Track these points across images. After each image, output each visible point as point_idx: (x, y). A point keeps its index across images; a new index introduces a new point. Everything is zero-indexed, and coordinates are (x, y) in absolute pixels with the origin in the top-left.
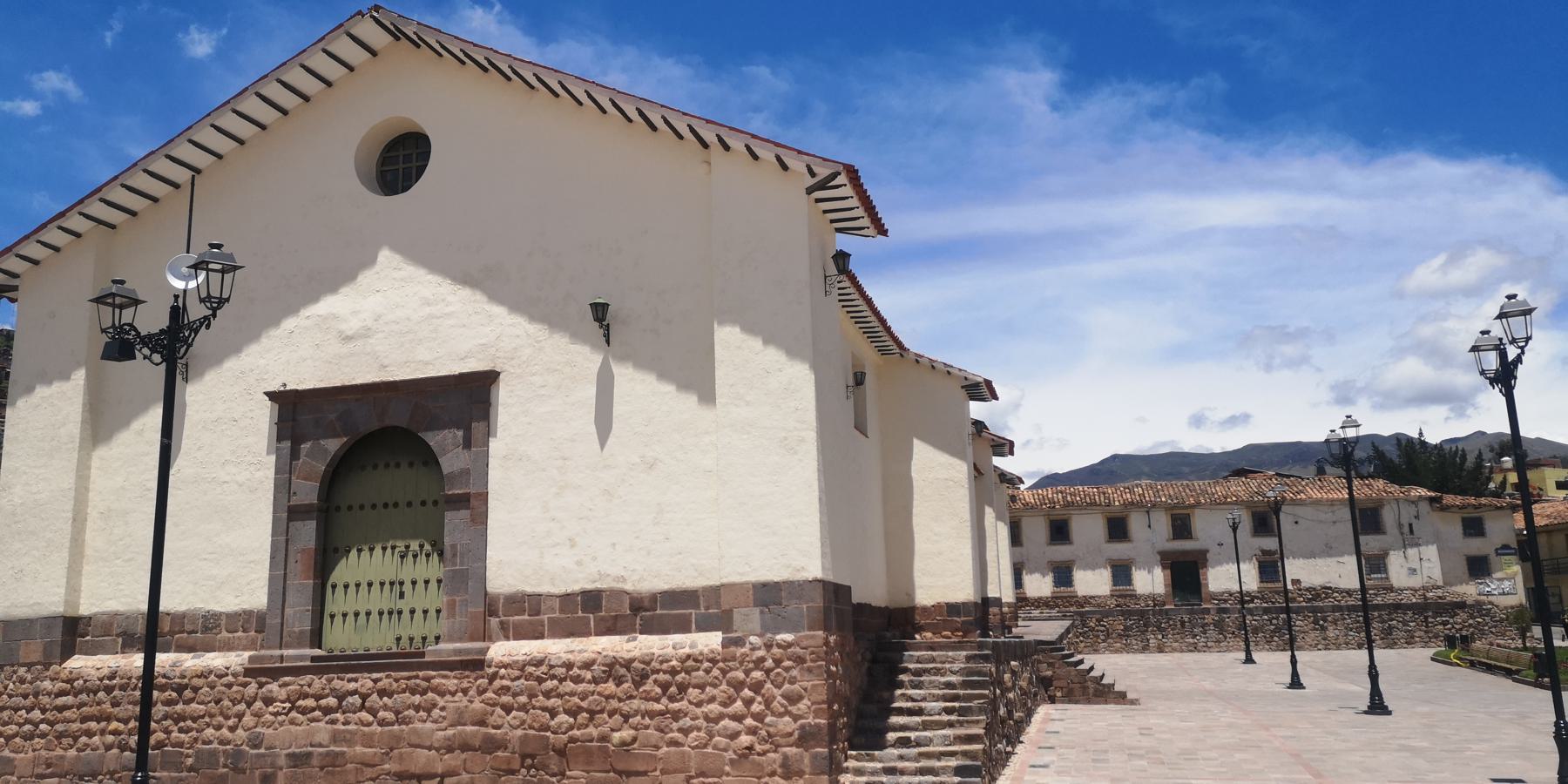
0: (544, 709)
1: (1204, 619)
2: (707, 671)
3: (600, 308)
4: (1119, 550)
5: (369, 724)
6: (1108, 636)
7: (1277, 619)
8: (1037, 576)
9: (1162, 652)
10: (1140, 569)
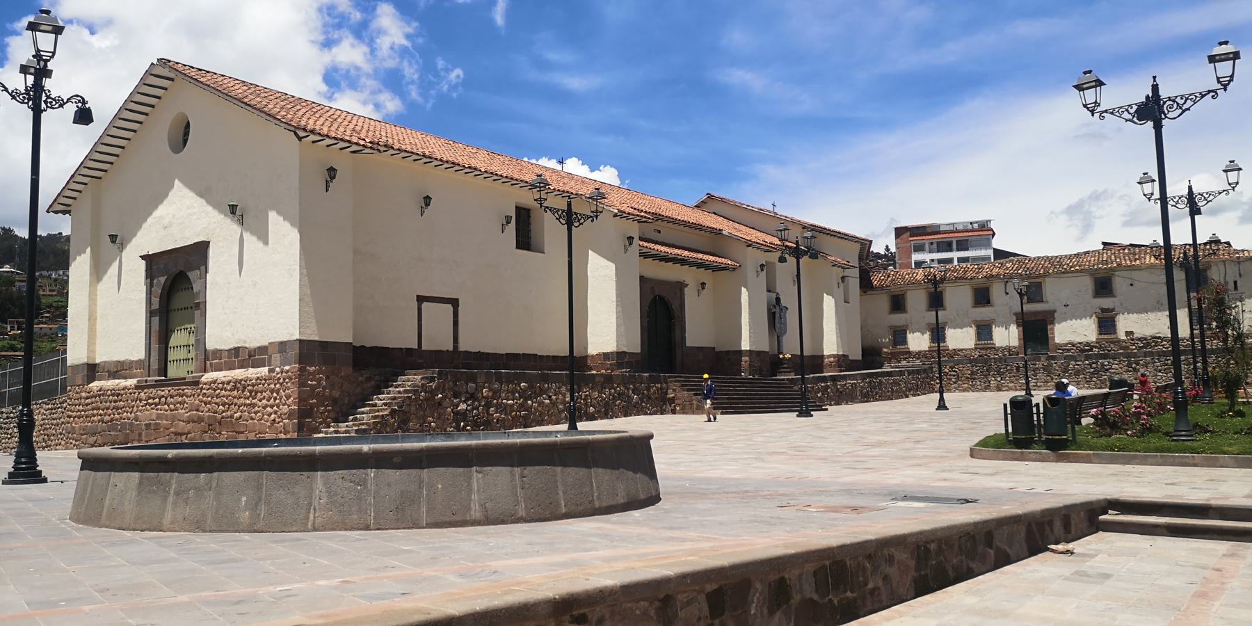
0: (216, 403)
1: (1035, 364)
2: (263, 385)
3: (235, 208)
4: (984, 313)
5: (167, 411)
6: (958, 378)
7: (1096, 363)
8: (918, 334)
9: (1000, 391)
10: (999, 327)
